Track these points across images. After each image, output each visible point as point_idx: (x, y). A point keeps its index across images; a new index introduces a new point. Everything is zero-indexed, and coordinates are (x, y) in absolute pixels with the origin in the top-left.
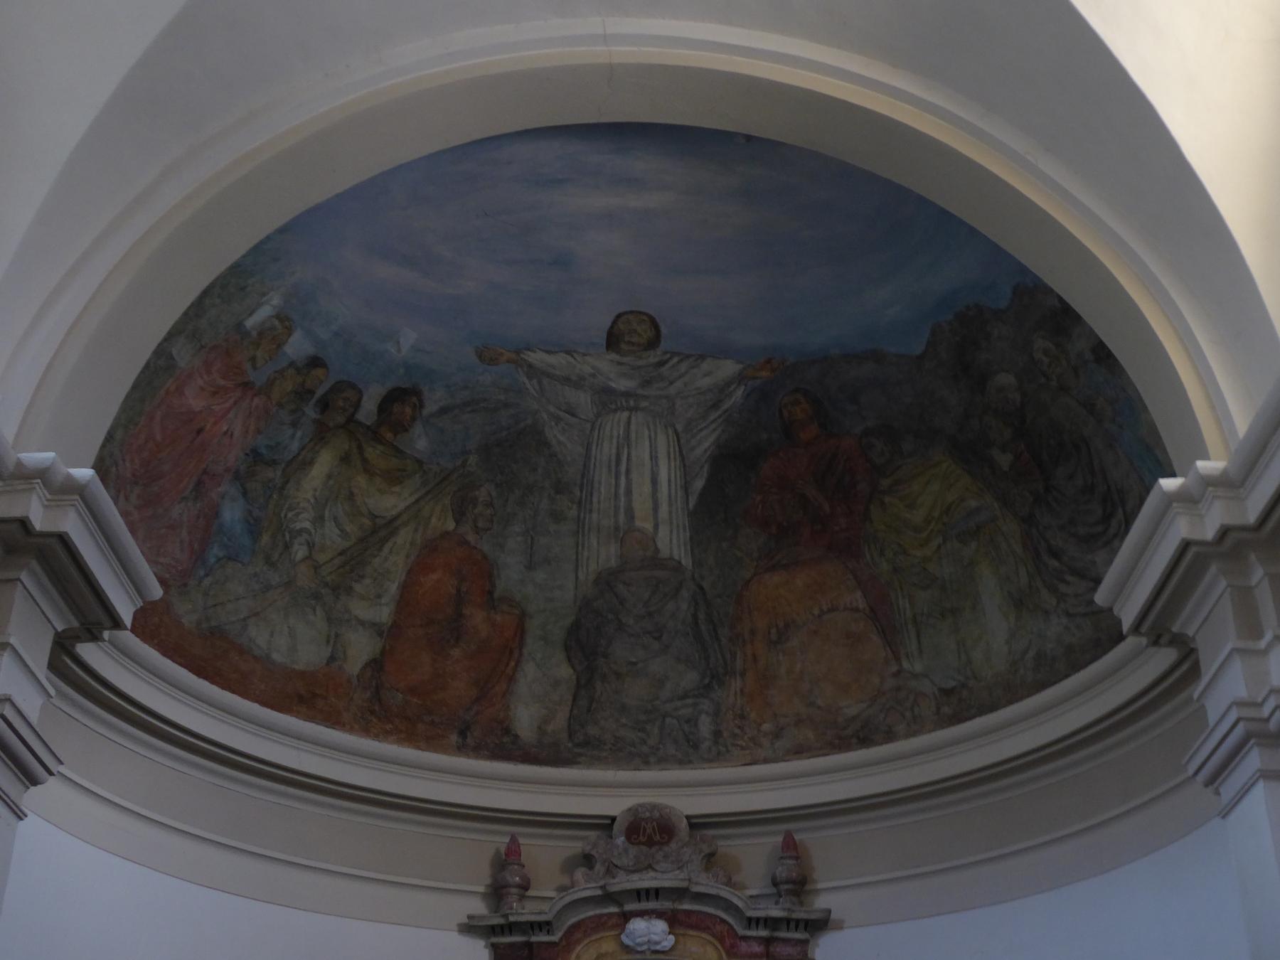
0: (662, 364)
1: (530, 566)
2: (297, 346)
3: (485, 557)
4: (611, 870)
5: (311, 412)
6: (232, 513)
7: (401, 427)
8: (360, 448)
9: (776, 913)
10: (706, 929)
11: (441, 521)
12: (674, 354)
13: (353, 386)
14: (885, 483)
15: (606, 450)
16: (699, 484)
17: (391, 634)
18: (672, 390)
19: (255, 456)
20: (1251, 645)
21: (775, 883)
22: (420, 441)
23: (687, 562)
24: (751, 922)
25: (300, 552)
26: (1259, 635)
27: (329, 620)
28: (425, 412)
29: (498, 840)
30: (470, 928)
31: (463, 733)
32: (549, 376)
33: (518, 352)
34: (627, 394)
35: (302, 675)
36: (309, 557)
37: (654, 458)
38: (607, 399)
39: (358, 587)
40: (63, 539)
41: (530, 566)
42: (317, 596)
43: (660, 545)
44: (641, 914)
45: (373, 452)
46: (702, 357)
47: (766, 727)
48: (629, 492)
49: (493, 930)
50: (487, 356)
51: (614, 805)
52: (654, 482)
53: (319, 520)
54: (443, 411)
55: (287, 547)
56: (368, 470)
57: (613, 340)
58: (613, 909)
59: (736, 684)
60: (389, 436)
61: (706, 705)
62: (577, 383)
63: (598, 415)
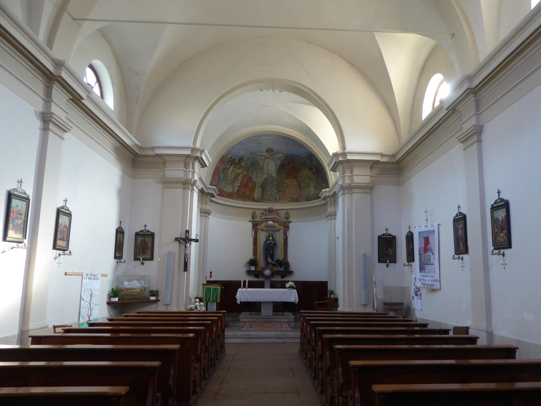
0: (273, 154)
1: (256, 178)
2: (229, 156)
3: (251, 177)
4: (266, 215)
5: (230, 163)
6: (222, 176)
7: (241, 163)
8: (236, 166)
9: (285, 221)
10: (277, 222)
11: (245, 173)
12: (275, 153)
13: (235, 159)
14: (301, 170)
15: (266, 163)
16: (278, 168)
17: (240, 187)
18: (274, 157)
19: (224, 169)
20: (330, 206)
21: (285, 217)
22: (243, 164)
23: (276, 177)
24: (282, 222)
25: (229, 179)
26: (331, 205)
27: (233, 186)
28: (244, 160)
29: (253, 211)
30: (250, 221)
31: (248, 198)
32: (259, 155)
33: (255, 153)
34: (269, 157)
35: (229, 193)
36: (230, 179)
37: (272, 165)
38: (266, 158)
39: (236, 182)
40: (213, 194)
41: (256, 178)
42: (231, 183)
43: (273, 175)
44: (269, 220)
45: (238, 166)
46: (278, 153)
47: (285, 198)
48: (269, 169)
49: (252, 222)
50: (251, 154)
51: (266, 207)
52: (272, 167)
53: (231, 174)
54: (246, 160)
55: (228, 178)
56: (237, 168)
57: (267, 151)
58: (266, 220)
59: (281, 192)
60: (239, 164)
61: (278, 195)
62: (262, 156)
63: (265, 160)
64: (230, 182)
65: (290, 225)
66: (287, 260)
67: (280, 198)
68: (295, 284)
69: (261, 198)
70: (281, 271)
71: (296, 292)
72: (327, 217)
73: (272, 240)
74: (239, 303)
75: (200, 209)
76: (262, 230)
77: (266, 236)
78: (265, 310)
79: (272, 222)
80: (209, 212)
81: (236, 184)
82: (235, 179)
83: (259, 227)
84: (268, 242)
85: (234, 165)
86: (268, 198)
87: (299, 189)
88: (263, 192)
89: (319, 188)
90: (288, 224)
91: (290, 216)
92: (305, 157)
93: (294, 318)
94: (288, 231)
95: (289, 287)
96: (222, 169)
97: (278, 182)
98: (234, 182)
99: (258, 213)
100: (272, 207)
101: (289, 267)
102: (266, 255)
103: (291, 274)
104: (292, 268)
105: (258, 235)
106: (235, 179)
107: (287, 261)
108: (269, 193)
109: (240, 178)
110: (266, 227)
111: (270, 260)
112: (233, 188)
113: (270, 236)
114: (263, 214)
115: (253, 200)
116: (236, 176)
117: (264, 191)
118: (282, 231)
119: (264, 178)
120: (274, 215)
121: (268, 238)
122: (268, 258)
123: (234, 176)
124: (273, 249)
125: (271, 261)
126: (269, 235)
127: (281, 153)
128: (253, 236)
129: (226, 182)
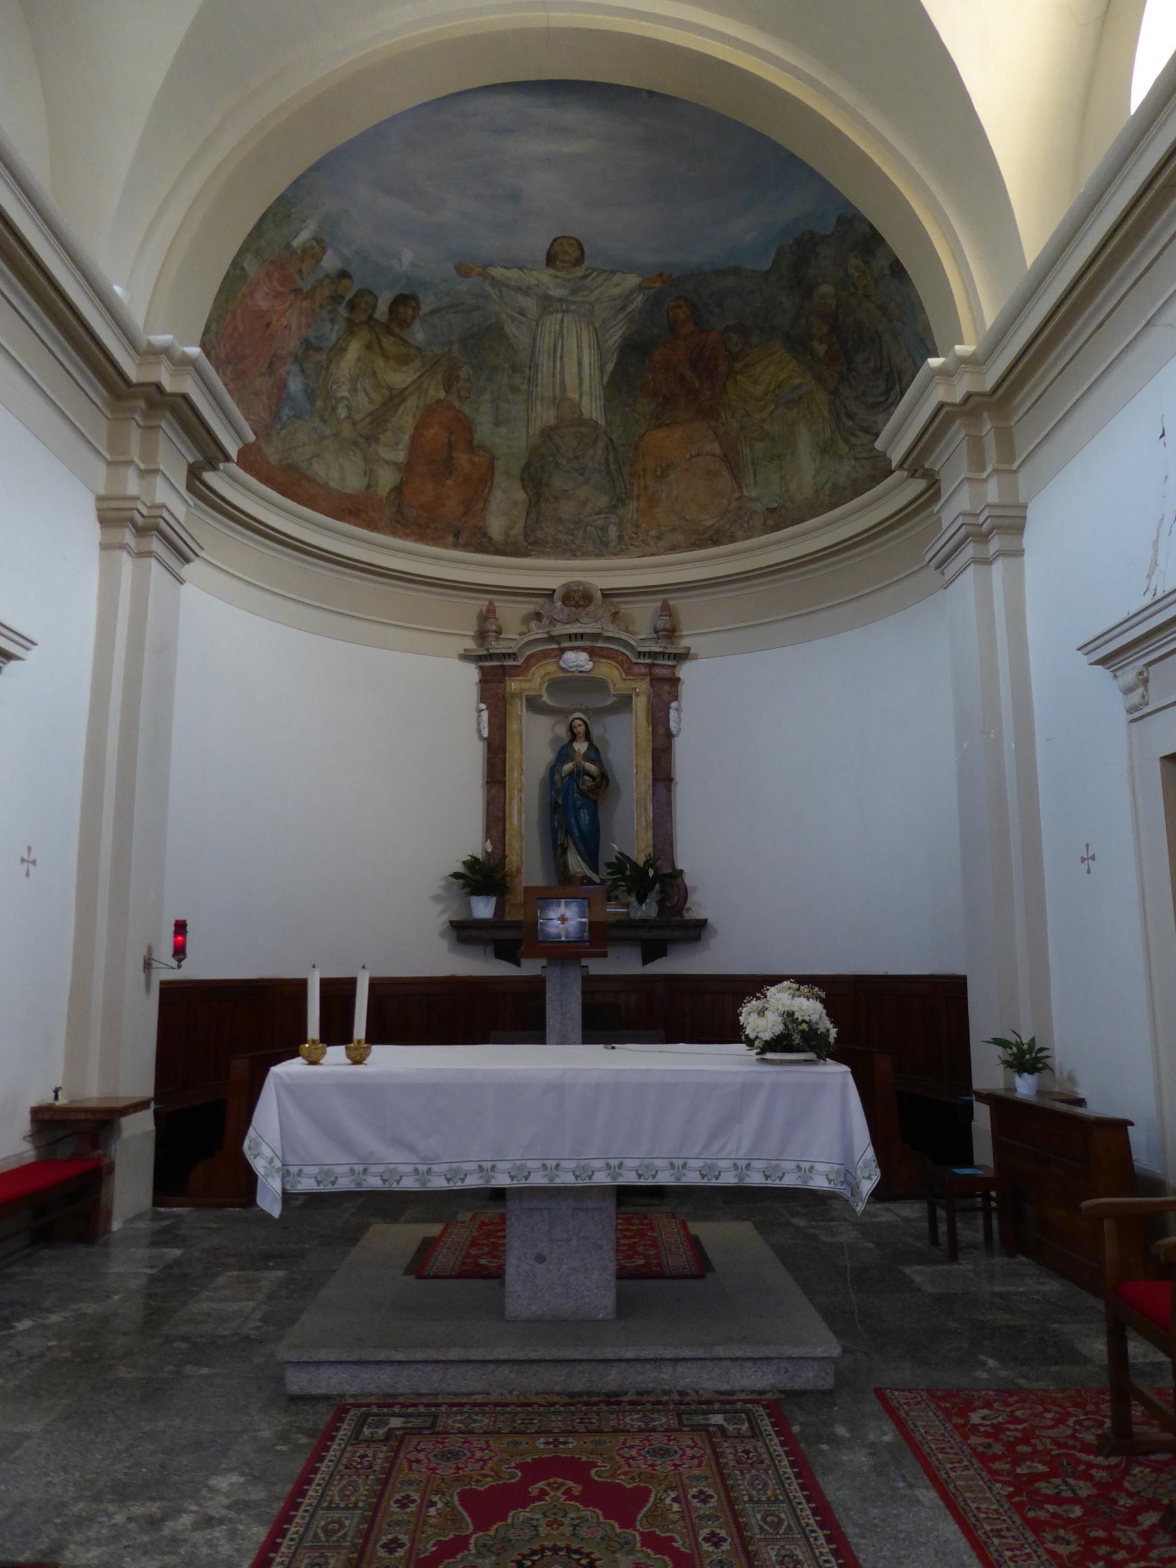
0: (585, 277)
2: (330, 262)
4: (553, 622)
5: (343, 311)
7: (405, 324)
8: (378, 338)
9: (656, 649)
10: (613, 658)
11: (436, 392)
12: (594, 270)
14: (738, 365)
15: (546, 343)
17: (407, 469)
18: (592, 297)
20: (976, 475)
21: (656, 631)
22: (418, 334)
23: (602, 422)
25: (343, 413)
27: (365, 459)
28: (422, 312)
30: (466, 657)
32: (507, 286)
34: (561, 300)
36: (349, 417)
37: (579, 347)
38: (547, 303)
40: (185, 398)
42: (356, 444)
44: (572, 649)
45: (387, 342)
46: (613, 272)
47: (653, 533)
49: (480, 658)
50: (463, 271)
51: (554, 582)
52: (580, 364)
53: (354, 390)
54: (434, 312)
55: (334, 409)
56: (385, 356)
57: (551, 259)
58: (555, 646)
59: (633, 505)
60: (397, 330)
61: (613, 518)
62: (526, 291)
63: (541, 316)
64: (347, 432)
65: (685, 671)
66: (672, 862)
67: (626, 538)
68: (829, 1005)
69: (526, 536)
70: (643, 923)
71: (844, 1086)
72: (938, 567)
73: (586, 757)
74: (276, 1211)
75: (100, 499)
76: (535, 705)
77: (556, 738)
78: (540, 1258)
79: (584, 656)
80: (163, 525)
81: (386, 454)
82: (379, 419)
83: (514, 685)
84: (568, 767)
85: (365, 335)
86: (563, 537)
87: (727, 475)
88: (534, 503)
89: (852, 447)
90: (674, 667)
91: (681, 626)
92: (768, 272)
93: (836, 1351)
94: (674, 705)
95: (780, 1043)
96: (293, 344)
97: (614, 448)
98: (371, 439)
99: (511, 614)
100: (582, 579)
101: (686, 898)
102: (555, 840)
103: (698, 939)
104: (700, 906)
105: (512, 727)
106: (379, 419)
107: (673, 867)
108: (567, 509)
109: (406, 418)
110: (557, 685)
111: (576, 863)
112: (370, 473)
113: (574, 737)
114: (538, 616)
115: (482, 543)
116: (384, 405)
117: (538, 501)
118: (640, 704)
119: (538, 424)
120: (596, 620)
121: (563, 748)
122: (565, 850)
123: (371, 401)
124: (595, 802)
125: (584, 866)
126: (571, 729)
127: (629, 268)
128: (486, 734)
129: (327, 431)
